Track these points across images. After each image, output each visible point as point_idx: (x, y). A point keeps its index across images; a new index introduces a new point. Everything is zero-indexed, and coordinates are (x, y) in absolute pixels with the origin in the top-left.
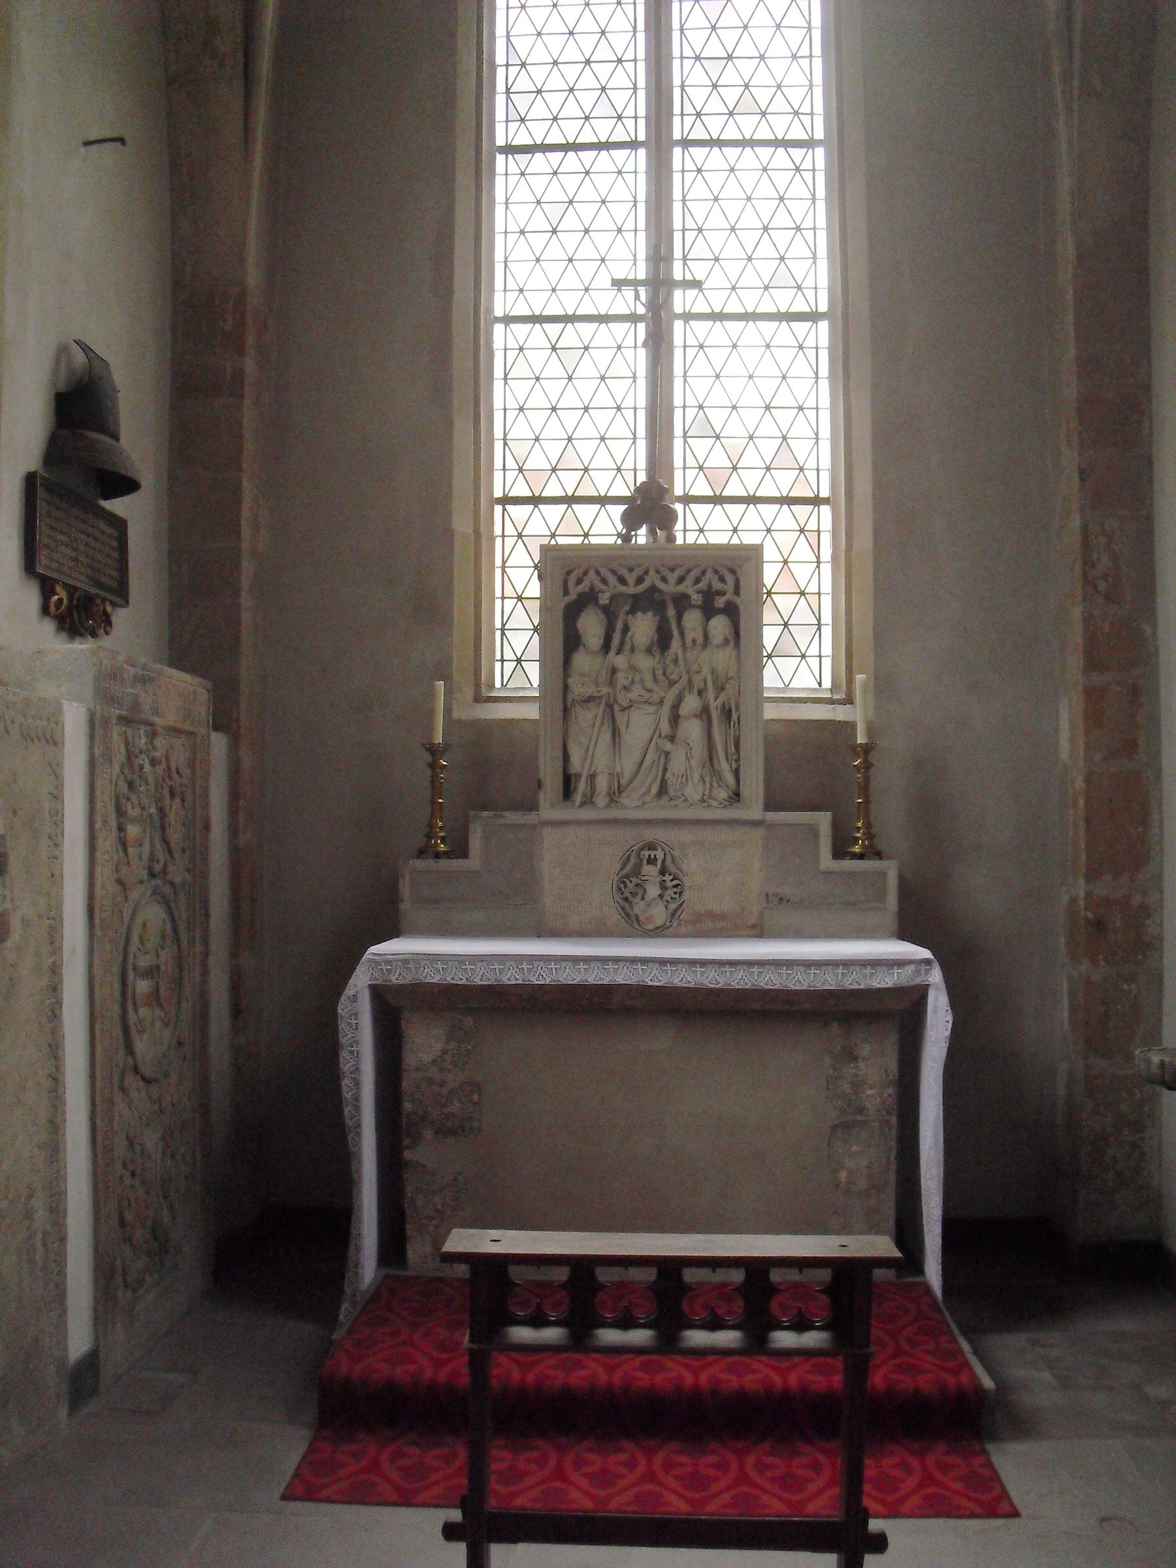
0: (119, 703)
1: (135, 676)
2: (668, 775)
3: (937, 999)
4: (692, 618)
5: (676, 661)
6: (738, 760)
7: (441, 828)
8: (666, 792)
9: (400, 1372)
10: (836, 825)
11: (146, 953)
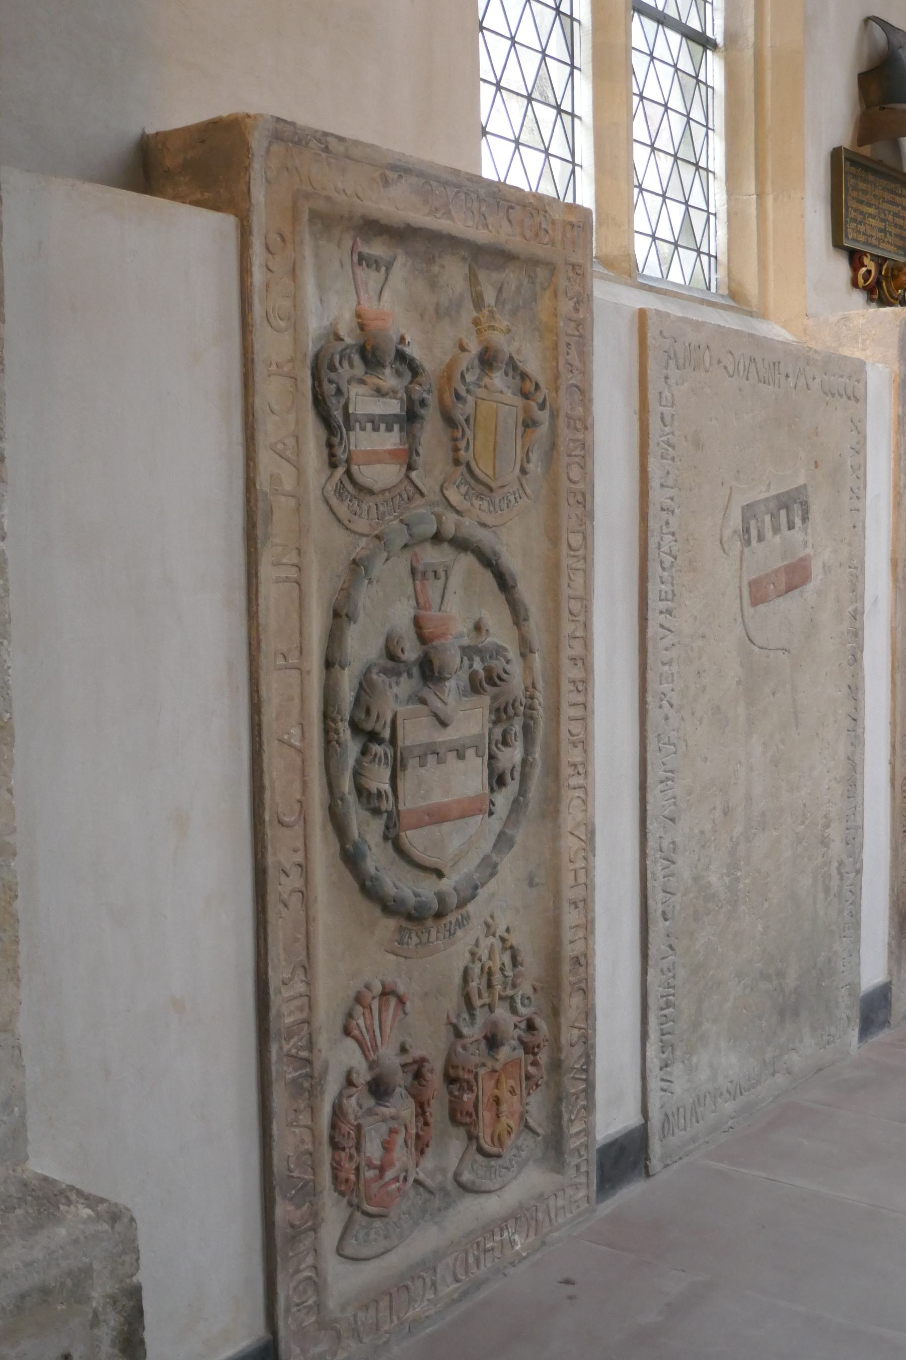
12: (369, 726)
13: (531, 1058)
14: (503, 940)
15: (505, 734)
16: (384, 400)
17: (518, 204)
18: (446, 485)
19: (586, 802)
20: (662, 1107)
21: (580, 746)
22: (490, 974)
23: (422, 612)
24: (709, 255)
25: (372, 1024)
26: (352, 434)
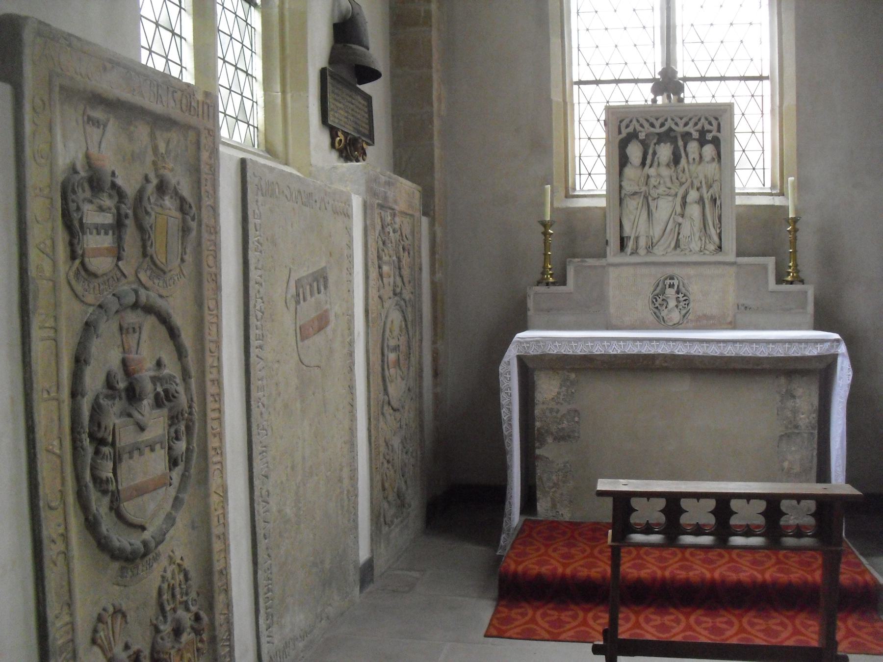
0: (377, 196)
1: (385, 182)
2: (681, 236)
3: (842, 363)
4: (693, 146)
5: (684, 171)
6: (720, 228)
7: (550, 269)
8: (679, 247)
9: (544, 570)
10: (777, 265)
11: (393, 338)
12: (100, 435)
13: (199, 637)
14: (179, 565)
15: (176, 432)
16: (103, 214)
17: (180, 90)
18: (139, 270)
19: (222, 471)
20: (268, 652)
21: (218, 435)
22: (173, 589)
23: (126, 355)
24: (254, 127)
25: (108, 634)
26: (85, 237)
